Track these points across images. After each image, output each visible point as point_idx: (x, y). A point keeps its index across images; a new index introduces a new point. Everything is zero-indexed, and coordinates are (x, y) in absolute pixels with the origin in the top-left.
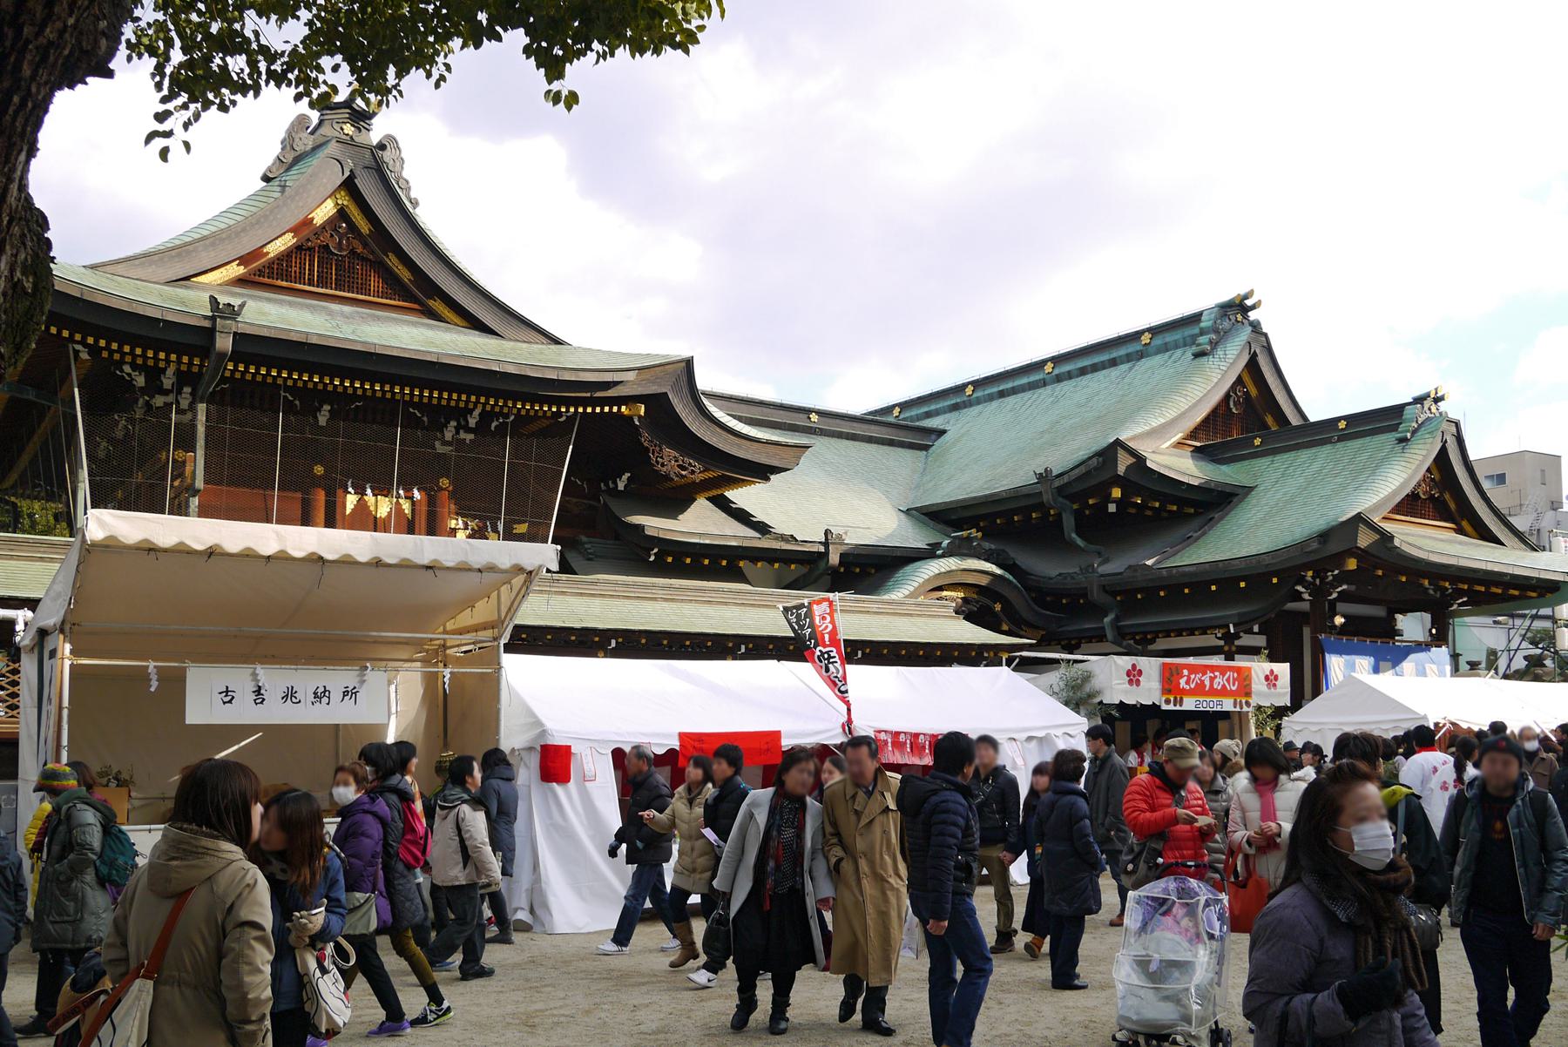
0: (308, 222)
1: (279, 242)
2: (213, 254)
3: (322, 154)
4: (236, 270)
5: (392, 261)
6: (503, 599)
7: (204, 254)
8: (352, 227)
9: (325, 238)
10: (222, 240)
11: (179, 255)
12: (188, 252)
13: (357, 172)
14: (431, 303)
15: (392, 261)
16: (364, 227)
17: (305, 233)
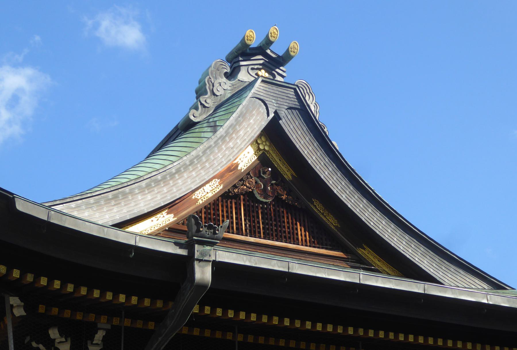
0: (232, 168)
1: (207, 188)
2: (149, 197)
3: (246, 100)
4: (165, 219)
5: (317, 208)
6: (135, 228)
7: (140, 197)
8: (276, 174)
9: (250, 184)
10: (157, 182)
11: (115, 197)
12: (125, 195)
13: (283, 113)
14: (360, 251)
15: (317, 208)
16: (287, 173)
17: (231, 178)
